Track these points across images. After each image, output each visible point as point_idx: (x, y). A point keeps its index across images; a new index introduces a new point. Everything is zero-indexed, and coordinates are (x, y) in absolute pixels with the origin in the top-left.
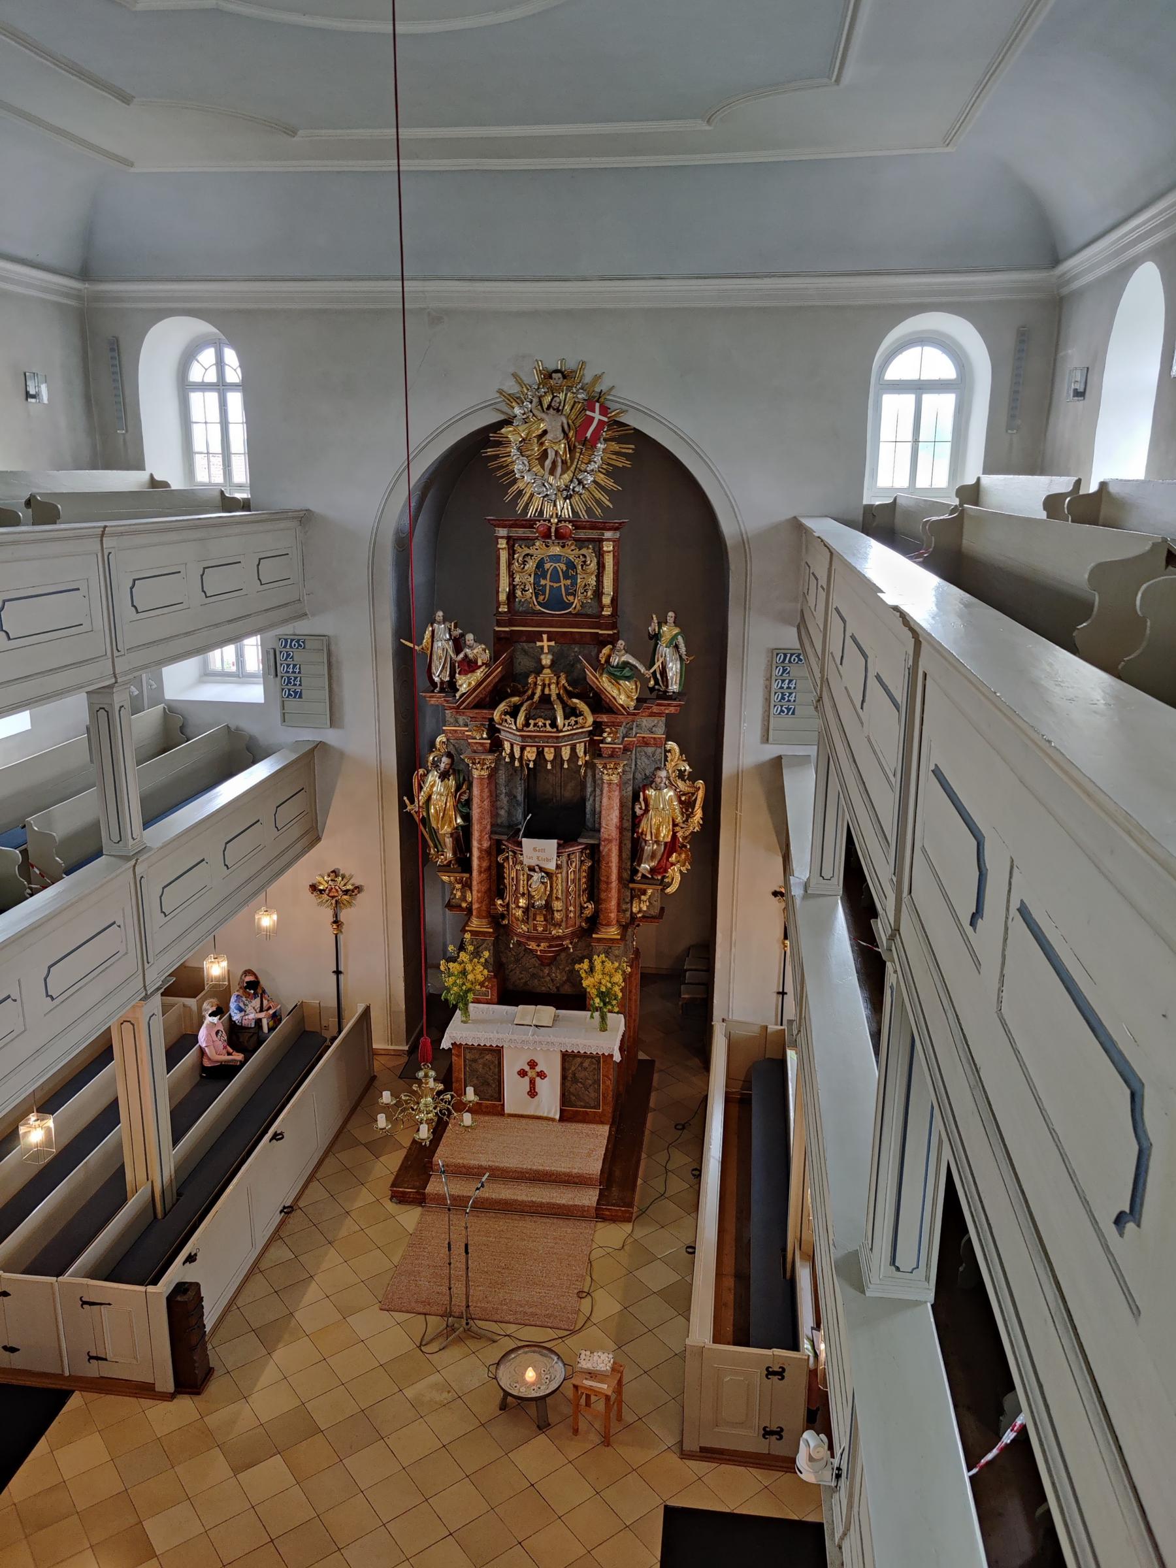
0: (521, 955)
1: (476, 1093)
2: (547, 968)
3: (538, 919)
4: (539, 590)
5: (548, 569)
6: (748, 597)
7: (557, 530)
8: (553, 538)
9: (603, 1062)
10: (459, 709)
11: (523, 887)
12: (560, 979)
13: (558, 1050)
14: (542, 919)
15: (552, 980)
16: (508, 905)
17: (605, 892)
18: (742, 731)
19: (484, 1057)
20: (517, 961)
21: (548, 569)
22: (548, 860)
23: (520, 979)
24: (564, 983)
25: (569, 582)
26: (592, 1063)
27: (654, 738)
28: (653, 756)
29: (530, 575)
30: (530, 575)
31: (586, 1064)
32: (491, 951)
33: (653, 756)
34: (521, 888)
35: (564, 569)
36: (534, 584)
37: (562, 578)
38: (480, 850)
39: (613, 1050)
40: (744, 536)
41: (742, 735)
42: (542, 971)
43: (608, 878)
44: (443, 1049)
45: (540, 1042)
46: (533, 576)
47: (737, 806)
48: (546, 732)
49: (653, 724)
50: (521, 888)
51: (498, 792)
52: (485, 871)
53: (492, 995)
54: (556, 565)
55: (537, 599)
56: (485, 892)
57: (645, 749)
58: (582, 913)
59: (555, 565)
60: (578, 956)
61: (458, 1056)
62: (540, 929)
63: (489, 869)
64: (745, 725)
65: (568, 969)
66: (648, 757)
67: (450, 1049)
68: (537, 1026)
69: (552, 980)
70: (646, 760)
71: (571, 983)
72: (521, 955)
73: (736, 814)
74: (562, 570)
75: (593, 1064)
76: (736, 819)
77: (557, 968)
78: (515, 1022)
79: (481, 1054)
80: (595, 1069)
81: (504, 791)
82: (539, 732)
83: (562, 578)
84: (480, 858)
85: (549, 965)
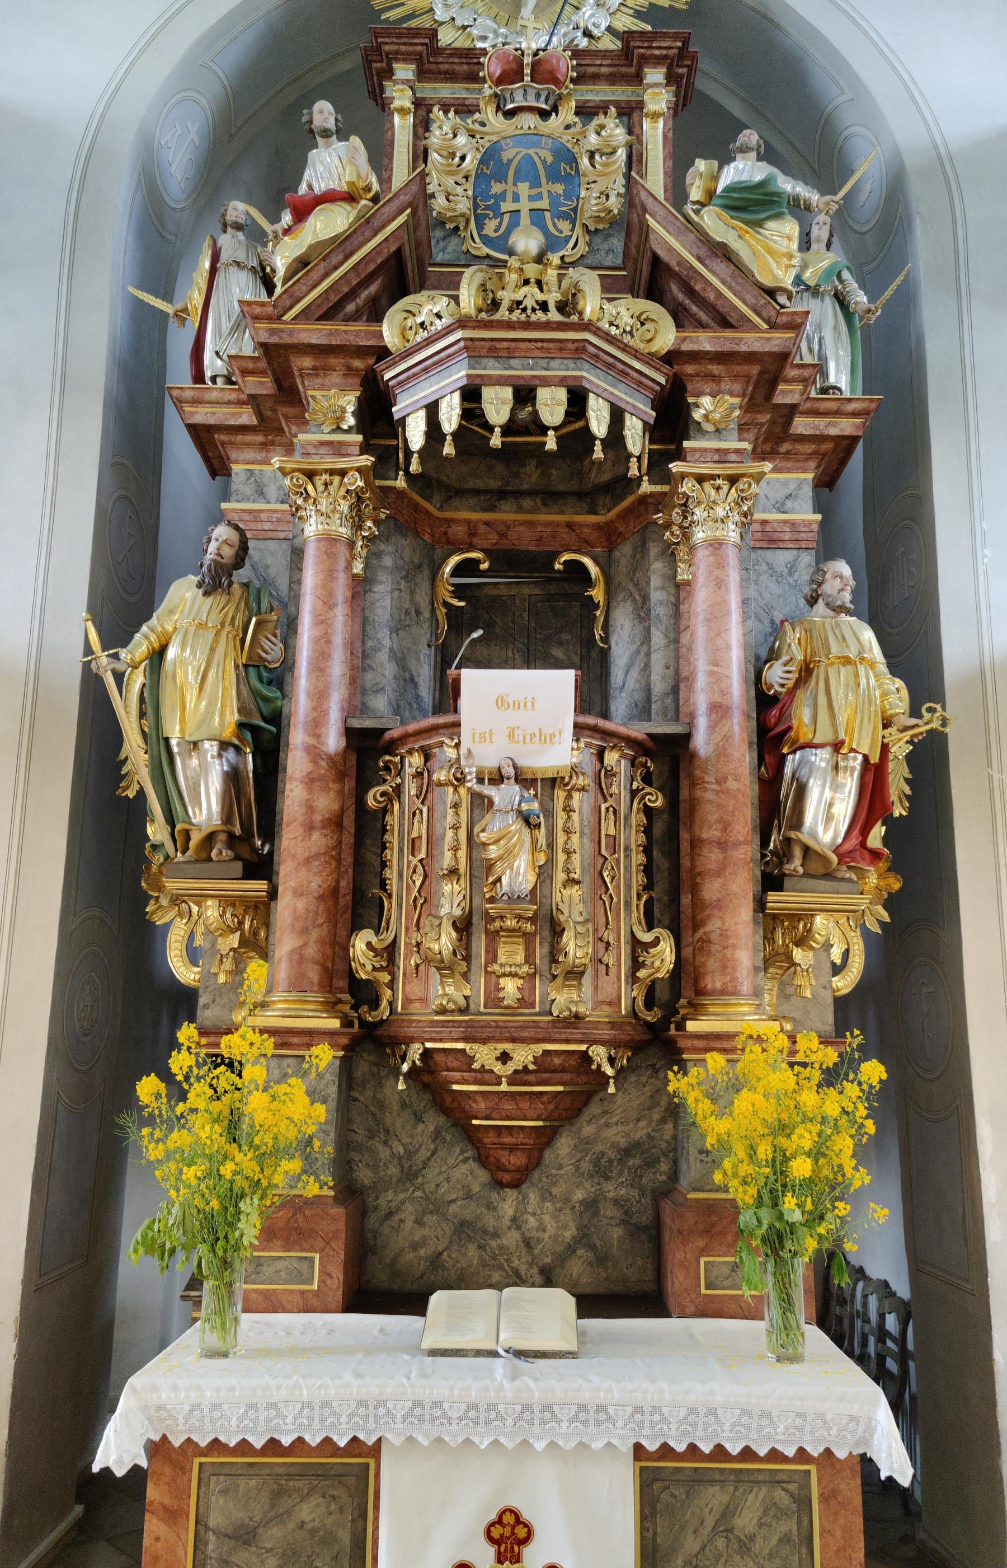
0: (424, 1154)
1: (886, 840)
2: (511, 1194)
3: (502, 958)
4: (487, 208)
5: (510, 161)
6: (962, 270)
7: (534, 66)
8: (527, 79)
9: (824, 1499)
10: (279, 318)
11: (455, 849)
12: (555, 1238)
13: (626, 1448)
14: (520, 958)
15: (528, 1244)
16: (391, 950)
17: (718, 874)
18: (981, 568)
19: (288, 1513)
20: (410, 1176)
21: (510, 161)
22: (547, 739)
23: (415, 1246)
24: (571, 1249)
25: (559, 188)
26: (771, 1510)
27: (793, 524)
28: (790, 574)
29: (467, 178)
30: (467, 178)
31: (746, 1521)
32: (333, 1104)
33: (790, 574)
34: (448, 855)
35: (550, 159)
36: (475, 198)
37: (543, 180)
38: (314, 753)
39: (870, 1430)
40: (942, 151)
41: (981, 578)
42: (490, 1207)
43: (726, 827)
44: (106, 1471)
45: (548, 1408)
46: (472, 180)
47: (989, 756)
48: (547, 326)
49: (786, 492)
50: (448, 855)
51: (370, 643)
52: (327, 823)
53: (324, 1273)
54: (531, 152)
55: (480, 227)
56: (321, 898)
57: (769, 555)
58: (636, 964)
59: (525, 151)
60: (614, 1145)
61: (173, 1515)
62: (510, 987)
63: (336, 823)
64: (987, 552)
65: (579, 1195)
66: (778, 577)
67: (136, 1473)
68: (520, 1354)
69: (528, 1244)
70: (773, 586)
71: (593, 1247)
72: (424, 1154)
73: (990, 778)
74: (544, 162)
75: (783, 1513)
76: (991, 789)
77: (546, 1195)
78: (427, 1344)
79: (278, 1494)
80: (785, 1539)
81: (387, 642)
82: (527, 326)
83: (543, 180)
84: (310, 781)
85: (516, 1185)
